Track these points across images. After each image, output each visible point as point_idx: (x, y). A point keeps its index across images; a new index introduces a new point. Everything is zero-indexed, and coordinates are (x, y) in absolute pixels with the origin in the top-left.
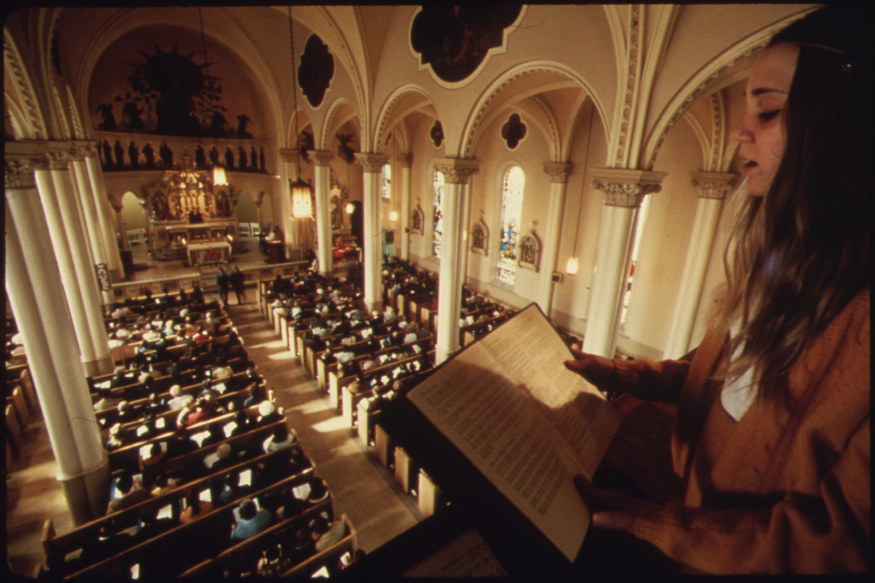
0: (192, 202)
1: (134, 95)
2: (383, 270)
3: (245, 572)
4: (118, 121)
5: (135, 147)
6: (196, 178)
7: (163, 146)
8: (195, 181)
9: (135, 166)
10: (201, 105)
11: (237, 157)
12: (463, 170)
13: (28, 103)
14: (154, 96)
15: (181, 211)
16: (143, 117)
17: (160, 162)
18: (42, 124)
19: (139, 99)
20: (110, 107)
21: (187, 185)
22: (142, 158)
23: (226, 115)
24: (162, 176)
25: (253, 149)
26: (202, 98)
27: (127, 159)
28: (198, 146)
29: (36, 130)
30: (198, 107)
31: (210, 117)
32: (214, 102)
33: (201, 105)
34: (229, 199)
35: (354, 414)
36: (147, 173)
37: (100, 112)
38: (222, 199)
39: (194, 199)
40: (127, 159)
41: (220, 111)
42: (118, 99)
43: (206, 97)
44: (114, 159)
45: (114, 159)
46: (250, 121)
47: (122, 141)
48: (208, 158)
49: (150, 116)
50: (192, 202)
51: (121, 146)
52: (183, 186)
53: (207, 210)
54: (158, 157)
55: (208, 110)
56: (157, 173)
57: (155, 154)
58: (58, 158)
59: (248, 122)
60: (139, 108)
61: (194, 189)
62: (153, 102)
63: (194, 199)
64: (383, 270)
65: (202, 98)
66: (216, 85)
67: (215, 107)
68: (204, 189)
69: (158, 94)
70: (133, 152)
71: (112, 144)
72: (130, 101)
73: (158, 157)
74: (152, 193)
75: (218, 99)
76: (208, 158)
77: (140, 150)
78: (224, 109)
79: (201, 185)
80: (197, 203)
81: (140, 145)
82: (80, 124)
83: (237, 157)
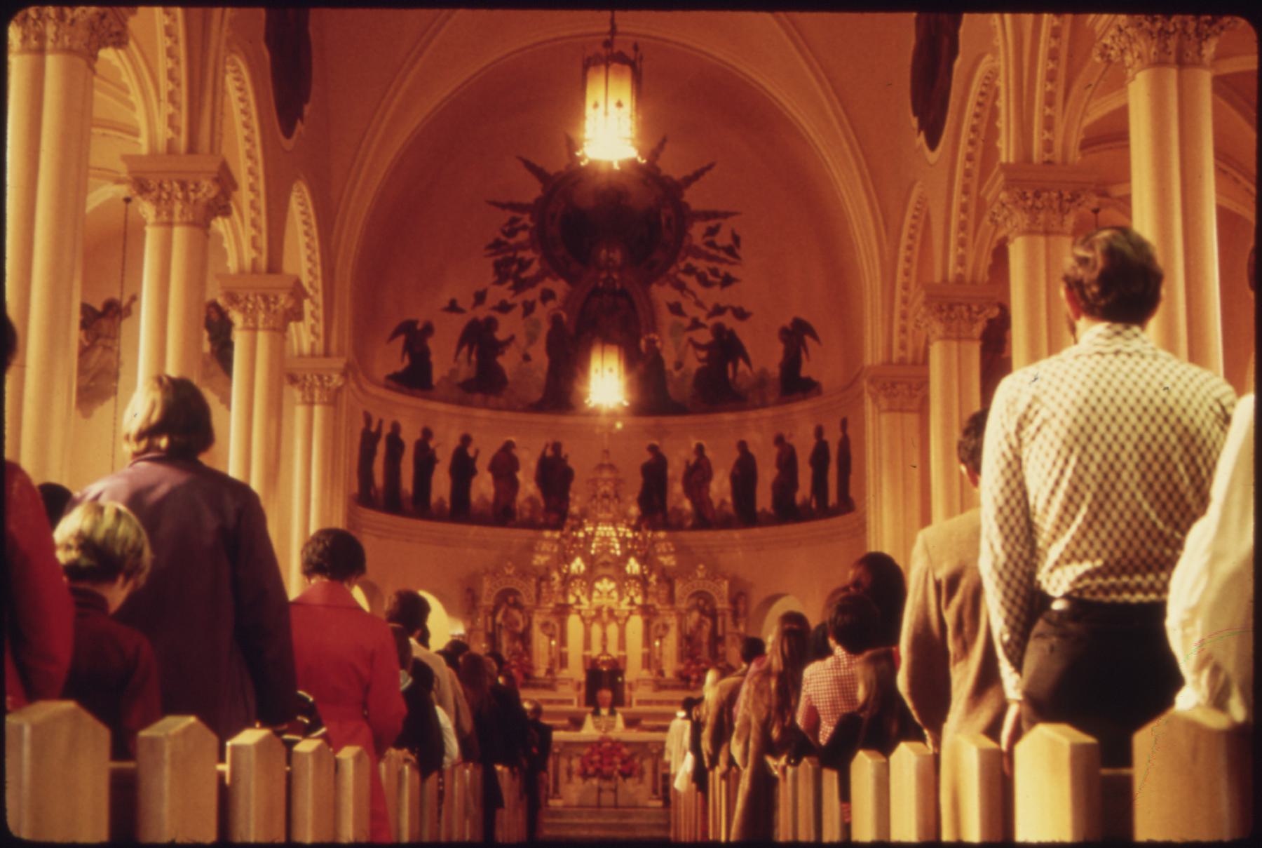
0: (604, 638)
1: (502, 292)
2: (958, 233)
5: (471, 452)
6: (623, 541)
7: (549, 453)
9: (460, 510)
10: (676, 309)
11: (767, 475)
13: (171, 76)
14: (547, 295)
15: (563, 661)
17: (531, 499)
18: (183, 122)
19: (504, 308)
20: (429, 329)
21: (590, 561)
22: (483, 486)
23: (744, 332)
24: (530, 549)
25: (819, 432)
26: (681, 286)
27: (441, 485)
29: (170, 134)
30: (666, 318)
31: (698, 346)
32: (715, 296)
33: (676, 309)
34: (726, 625)
37: (401, 340)
38: (699, 625)
39: (613, 630)
40: (441, 485)
41: (728, 320)
42: (453, 307)
43: (691, 282)
44: (407, 482)
45: (407, 482)
47: (438, 430)
48: (677, 488)
49: (526, 358)
50: (604, 638)
51: (432, 444)
52: (578, 565)
54: (528, 486)
55: (696, 324)
56: (518, 536)
57: (520, 476)
58: (192, 195)
60: (501, 335)
61: (611, 578)
62: (542, 313)
64: (958, 233)
65: (681, 286)
68: (642, 580)
69: (560, 287)
70: (463, 468)
72: (482, 313)
73: (528, 486)
74: (488, 593)
75: (728, 281)
76: (677, 488)
77: (482, 464)
78: (741, 314)
79: (633, 566)
80: (622, 644)
81: (485, 451)
82: (320, 313)
83: (767, 475)
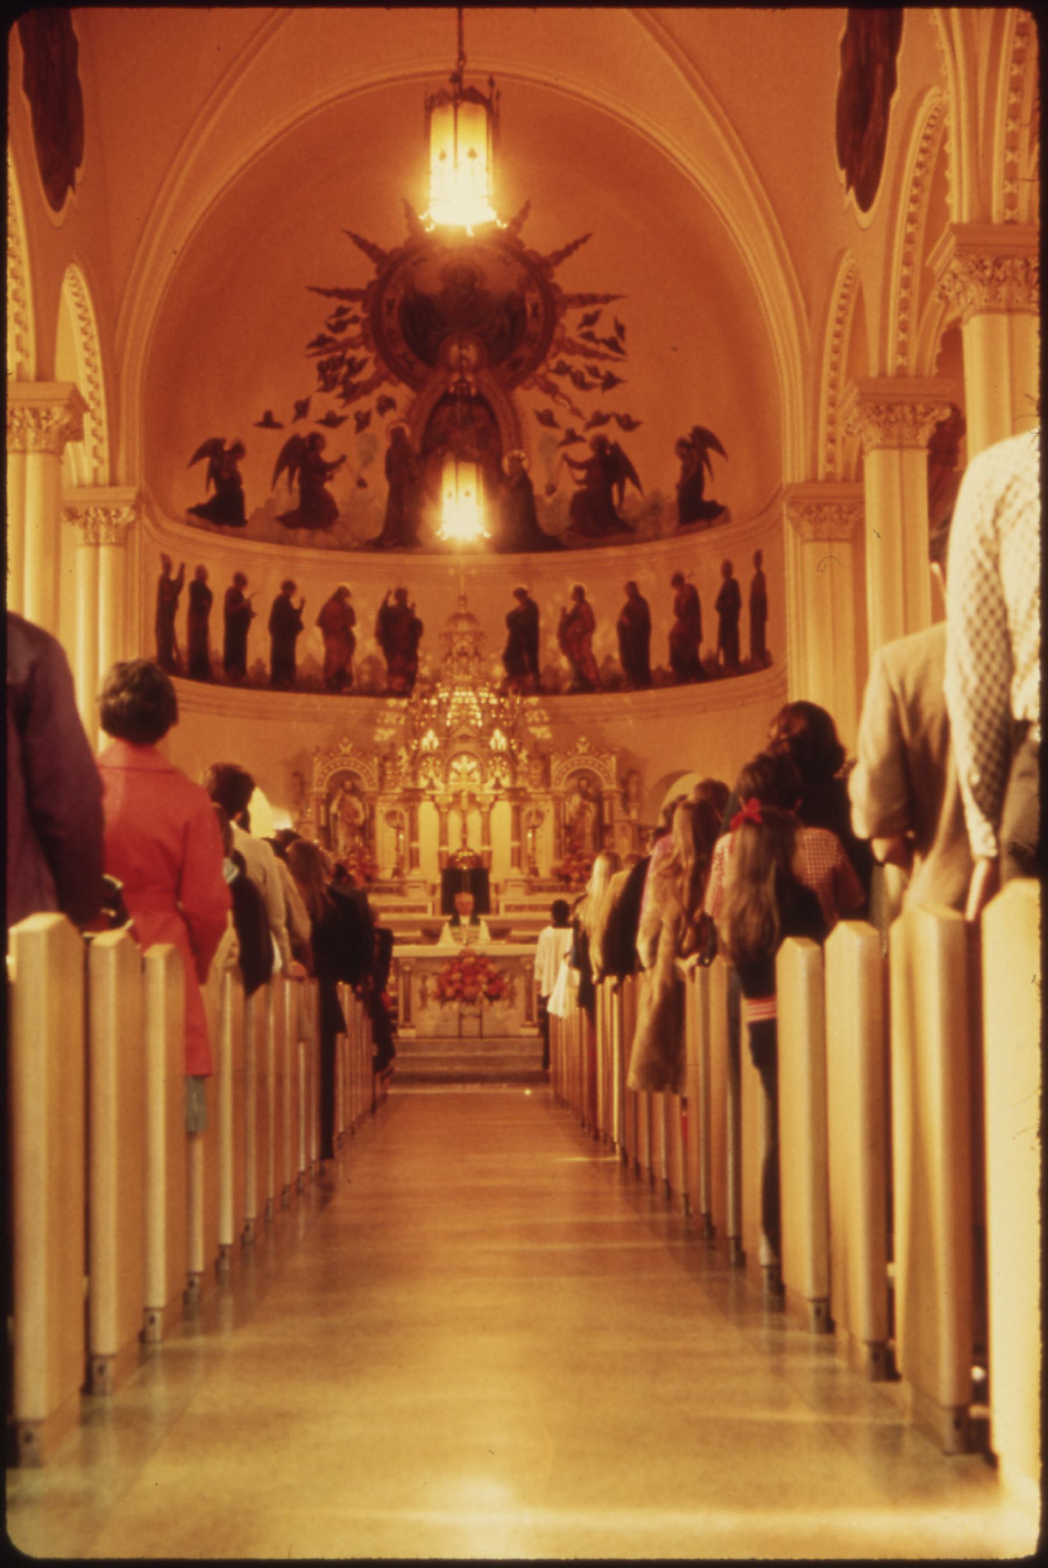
3: (111, 885)
4: (252, 503)
6: (486, 708)
7: (392, 602)
8: (478, 720)
10: (547, 419)
12: (998, 264)
15: (414, 859)
16: (338, 488)
17: (370, 660)
19: (332, 421)
21: (447, 736)
23: (631, 445)
24: (371, 721)
25: (727, 569)
26: (551, 390)
28: (520, 594)
30: (535, 431)
33: (547, 419)
35: (464, 836)
36: (318, 702)
38: (582, 811)
39: (474, 819)
42: (268, 422)
43: (565, 384)
46: (720, 449)
47: (254, 577)
51: (246, 594)
53: (518, 857)
55: (572, 437)
57: (357, 630)
59: (712, 453)
60: (328, 455)
62: (380, 426)
63: (474, 819)
66: (604, 329)
67: (600, 419)
71: (219, 585)
72: (305, 428)
77: (310, 617)
78: (628, 424)
79: (499, 740)
82: (103, 431)
